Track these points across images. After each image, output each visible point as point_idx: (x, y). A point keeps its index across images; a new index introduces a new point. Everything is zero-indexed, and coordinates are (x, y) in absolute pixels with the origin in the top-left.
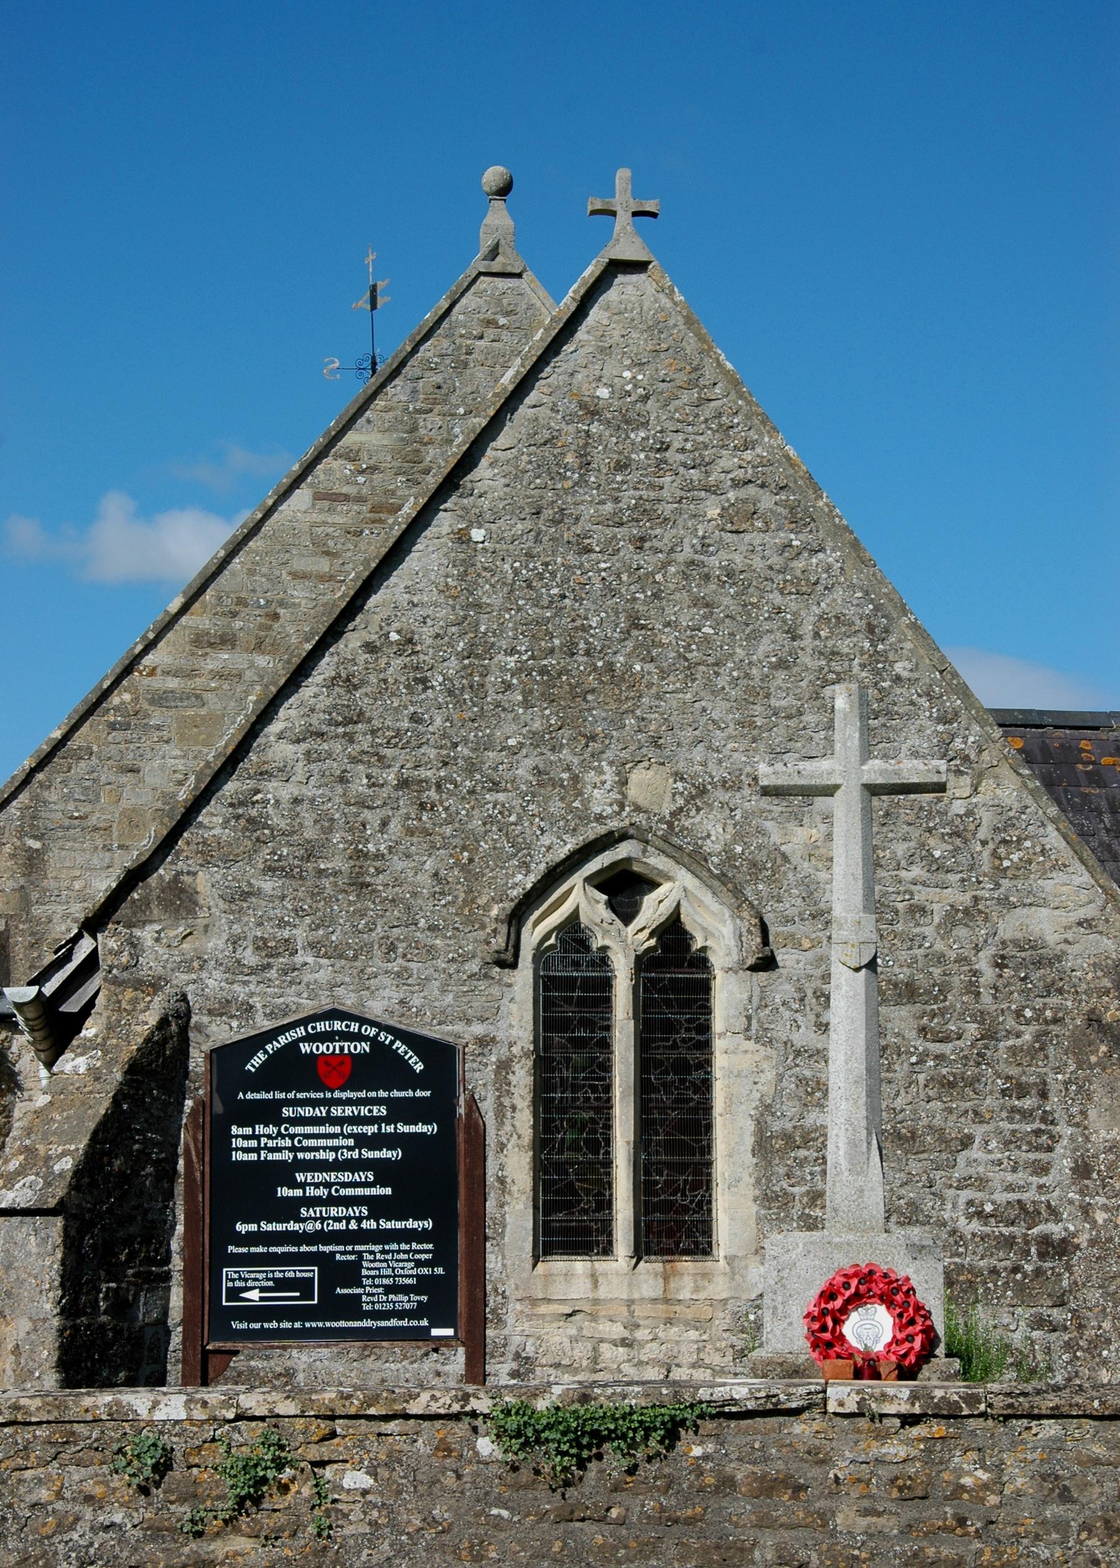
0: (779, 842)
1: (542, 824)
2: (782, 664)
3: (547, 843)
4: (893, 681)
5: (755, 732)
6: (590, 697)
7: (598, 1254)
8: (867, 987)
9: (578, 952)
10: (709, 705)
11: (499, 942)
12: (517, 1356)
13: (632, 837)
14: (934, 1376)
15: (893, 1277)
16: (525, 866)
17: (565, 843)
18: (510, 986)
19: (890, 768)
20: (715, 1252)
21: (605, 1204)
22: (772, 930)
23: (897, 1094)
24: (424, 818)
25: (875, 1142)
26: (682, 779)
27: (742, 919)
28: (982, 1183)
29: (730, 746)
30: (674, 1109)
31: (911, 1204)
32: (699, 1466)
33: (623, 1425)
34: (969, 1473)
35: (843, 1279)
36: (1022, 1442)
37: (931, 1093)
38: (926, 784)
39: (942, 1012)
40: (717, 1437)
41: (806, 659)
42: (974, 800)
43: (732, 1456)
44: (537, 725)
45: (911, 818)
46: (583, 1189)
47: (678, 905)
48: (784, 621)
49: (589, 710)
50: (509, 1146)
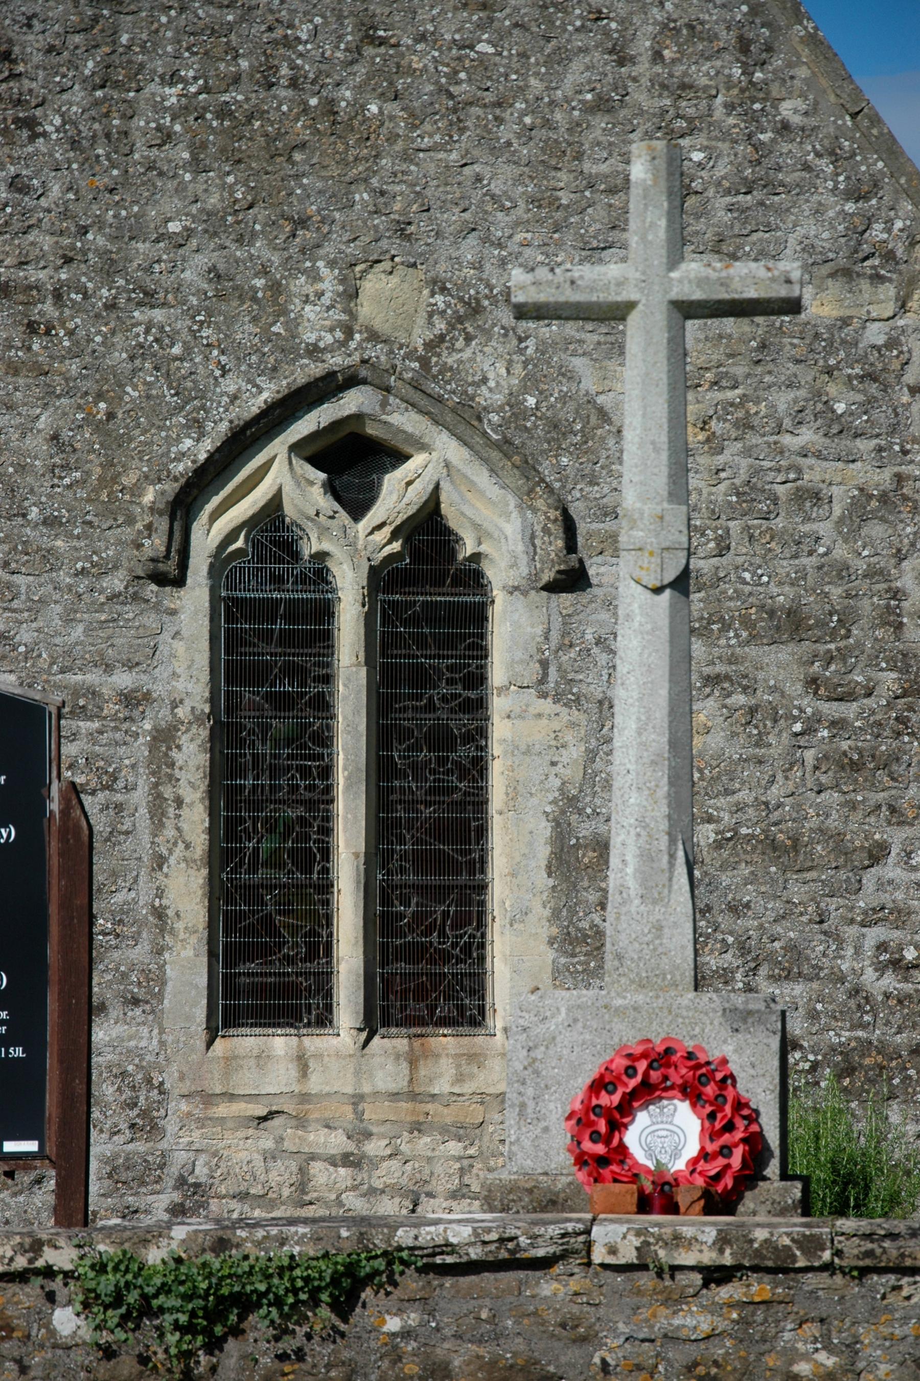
0: (593, 389)
1: (223, 359)
2: (602, 105)
3: (232, 389)
4: (777, 132)
5: (559, 215)
6: (298, 156)
7: (309, 1025)
8: (672, 617)
9: (281, 561)
10: (486, 172)
11: (156, 544)
12: (181, 1182)
13: (364, 382)
14: (763, 1209)
15: (702, 1059)
16: (197, 426)
17: (260, 391)
18: (173, 613)
19: (714, 275)
20: (489, 1021)
21: (320, 947)
22: (582, 528)
23: (772, 781)
24: (36, 347)
25: (681, 854)
26: (443, 290)
27: (535, 510)
28: (899, 916)
29: (519, 237)
30: (428, 804)
31: (791, 948)
32: (395, 1347)
33: (280, 1285)
34: (806, 1357)
35: (626, 1062)
36: (888, 1309)
37: (824, 779)
38: (769, 301)
39: (843, 655)
40: (422, 1301)
41: (640, 97)
42: (901, 323)
43: (447, 1332)
44: (213, 201)
45: (798, 353)
46: (287, 926)
47: (437, 487)
48: (607, 33)
49: (297, 177)
50: (172, 860)
